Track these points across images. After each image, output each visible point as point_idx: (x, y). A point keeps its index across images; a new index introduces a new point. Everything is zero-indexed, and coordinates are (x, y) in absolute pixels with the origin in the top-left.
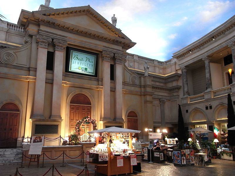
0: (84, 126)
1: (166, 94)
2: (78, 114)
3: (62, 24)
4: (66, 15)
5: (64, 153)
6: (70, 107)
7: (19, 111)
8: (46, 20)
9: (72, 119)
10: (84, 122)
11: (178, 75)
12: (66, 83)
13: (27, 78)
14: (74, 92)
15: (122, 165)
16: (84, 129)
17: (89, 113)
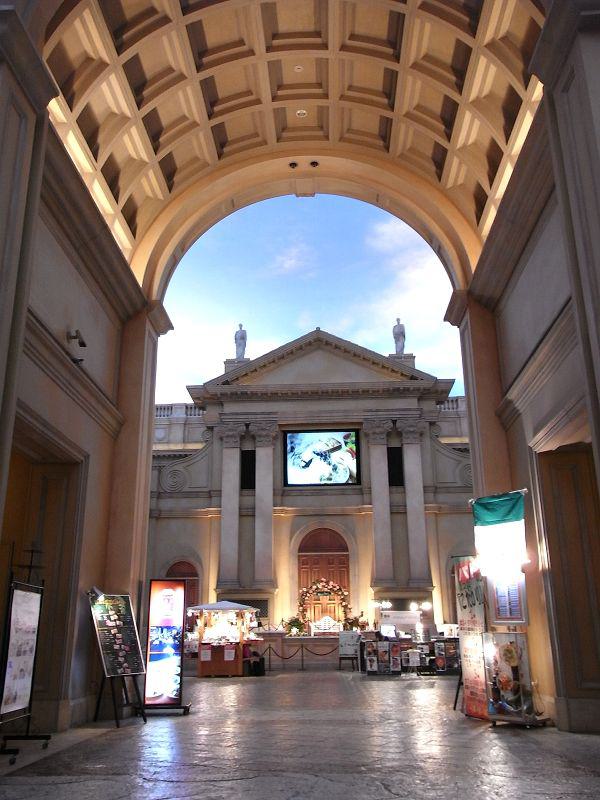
3: (260, 390)
4: (273, 365)
7: (196, 575)
12: (286, 512)
13: (207, 513)
15: (209, 658)
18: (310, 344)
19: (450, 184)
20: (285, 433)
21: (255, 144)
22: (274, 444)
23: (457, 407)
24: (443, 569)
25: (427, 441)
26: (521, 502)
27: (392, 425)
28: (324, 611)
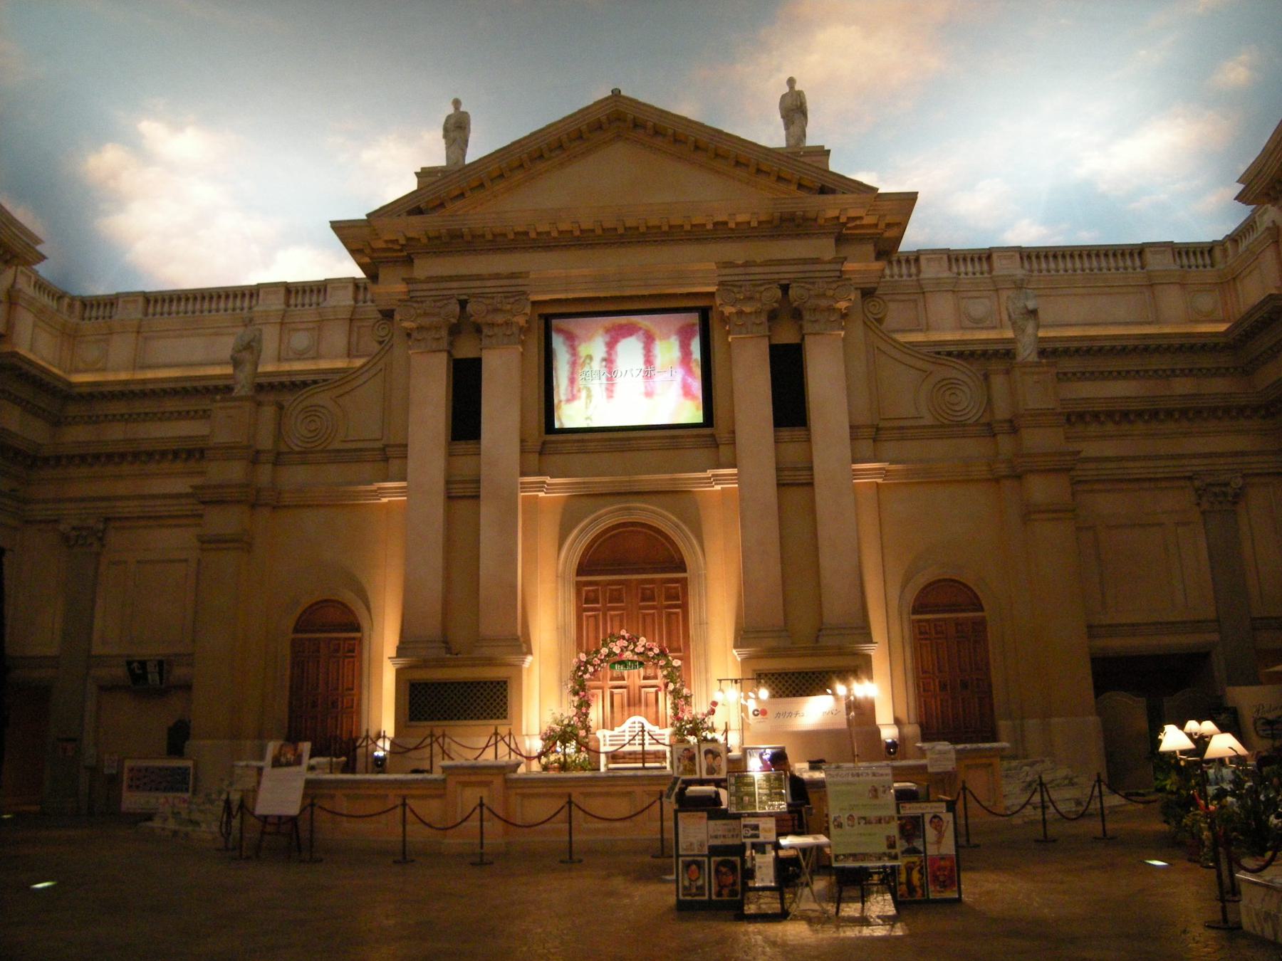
0: (655, 677)
1: (1241, 443)
2: (621, 621)
5: (570, 803)
6: (578, 593)
8: (443, 231)
10: (602, 661)
16: (657, 693)
17: (677, 614)
18: (599, 126)
20: (547, 319)
22: (523, 343)
23: (919, 272)
24: (894, 603)
25: (858, 331)
27: (779, 293)
28: (634, 703)
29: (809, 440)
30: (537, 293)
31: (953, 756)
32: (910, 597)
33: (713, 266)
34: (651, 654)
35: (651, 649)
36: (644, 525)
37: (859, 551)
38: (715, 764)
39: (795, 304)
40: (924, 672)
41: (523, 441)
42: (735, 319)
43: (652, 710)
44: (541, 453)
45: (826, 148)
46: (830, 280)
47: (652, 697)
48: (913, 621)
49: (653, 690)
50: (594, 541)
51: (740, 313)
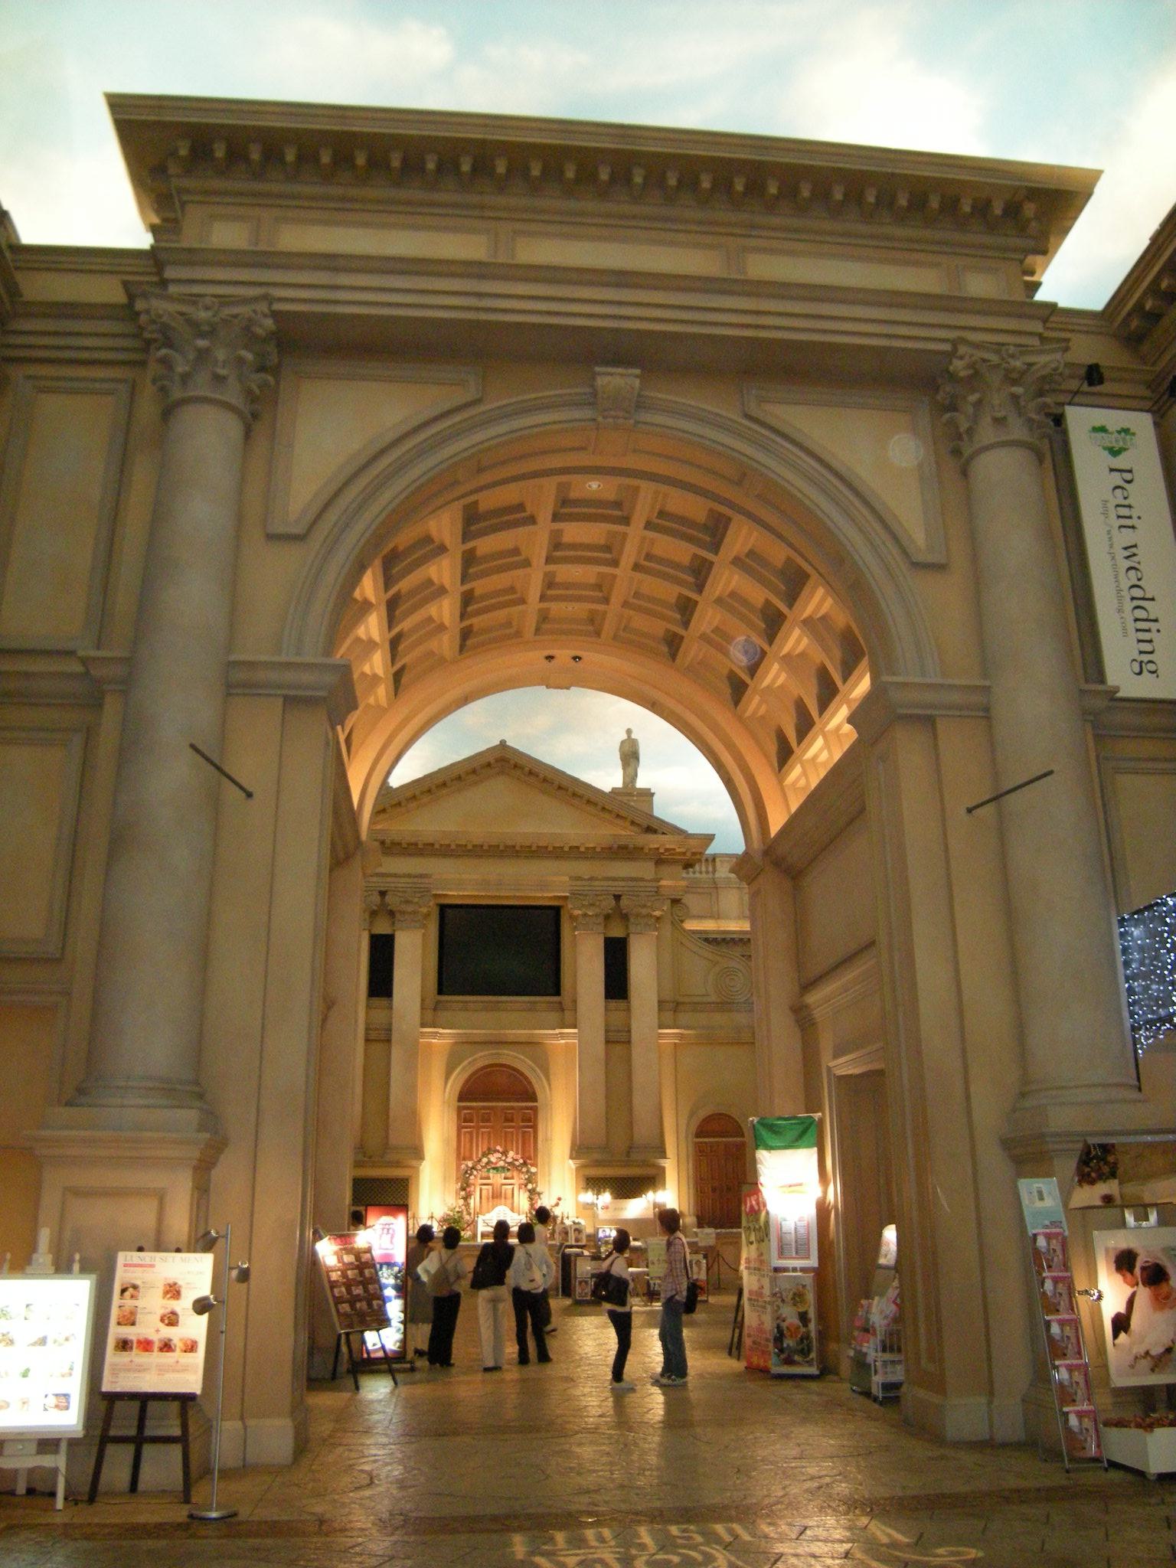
0: (512, 1178)
4: (425, 799)
9: (467, 1154)
11: (734, 936)
14: (469, 1063)
17: (529, 1132)
19: (748, 714)
21: (509, 636)
23: (714, 871)
24: (683, 1128)
25: (667, 930)
26: (813, 1130)
29: (628, 1010)
30: (437, 889)
31: (714, 1235)
32: (693, 1128)
33: (567, 879)
34: (517, 1163)
35: (517, 1160)
36: (508, 1067)
37: (660, 1093)
38: (580, 1236)
39: (624, 911)
40: (701, 1179)
41: (423, 1000)
42: (580, 919)
43: (509, 1201)
44: (435, 1009)
45: (652, 791)
46: (651, 894)
47: (510, 1192)
48: (696, 1143)
49: (511, 1187)
50: (471, 1076)
51: (585, 915)
